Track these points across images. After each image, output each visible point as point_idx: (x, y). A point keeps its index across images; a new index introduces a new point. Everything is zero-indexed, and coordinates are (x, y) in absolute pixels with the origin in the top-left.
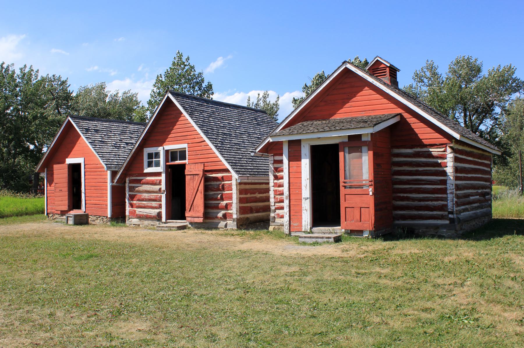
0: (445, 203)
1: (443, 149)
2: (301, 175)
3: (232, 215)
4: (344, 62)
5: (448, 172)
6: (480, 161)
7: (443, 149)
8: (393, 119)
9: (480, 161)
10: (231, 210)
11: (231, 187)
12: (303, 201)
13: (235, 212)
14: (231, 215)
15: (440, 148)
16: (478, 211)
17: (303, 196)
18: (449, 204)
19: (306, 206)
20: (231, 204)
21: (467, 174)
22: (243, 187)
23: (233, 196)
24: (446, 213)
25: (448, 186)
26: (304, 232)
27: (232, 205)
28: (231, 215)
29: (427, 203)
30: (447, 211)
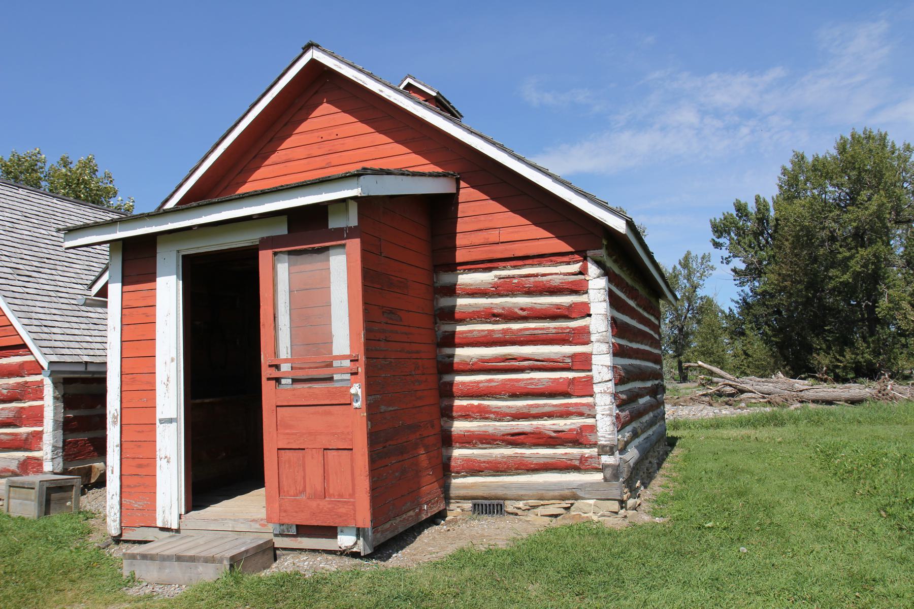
0: (590, 421)
1: (576, 267)
2: (154, 348)
3: (41, 465)
4: (306, 49)
5: (592, 329)
6: (646, 314)
7: (576, 267)
8: (430, 179)
9: (646, 314)
10: (40, 449)
11: (42, 392)
12: (160, 428)
13: (49, 456)
14: (38, 463)
15: (568, 263)
16: (650, 432)
17: (159, 416)
18: (600, 425)
19: (170, 443)
20: (39, 436)
21: (631, 341)
22: (73, 389)
23: (45, 414)
24: (594, 451)
25: (594, 373)
26: (163, 529)
27: (41, 438)
28: (38, 463)
29: (536, 423)
30: (595, 445)
